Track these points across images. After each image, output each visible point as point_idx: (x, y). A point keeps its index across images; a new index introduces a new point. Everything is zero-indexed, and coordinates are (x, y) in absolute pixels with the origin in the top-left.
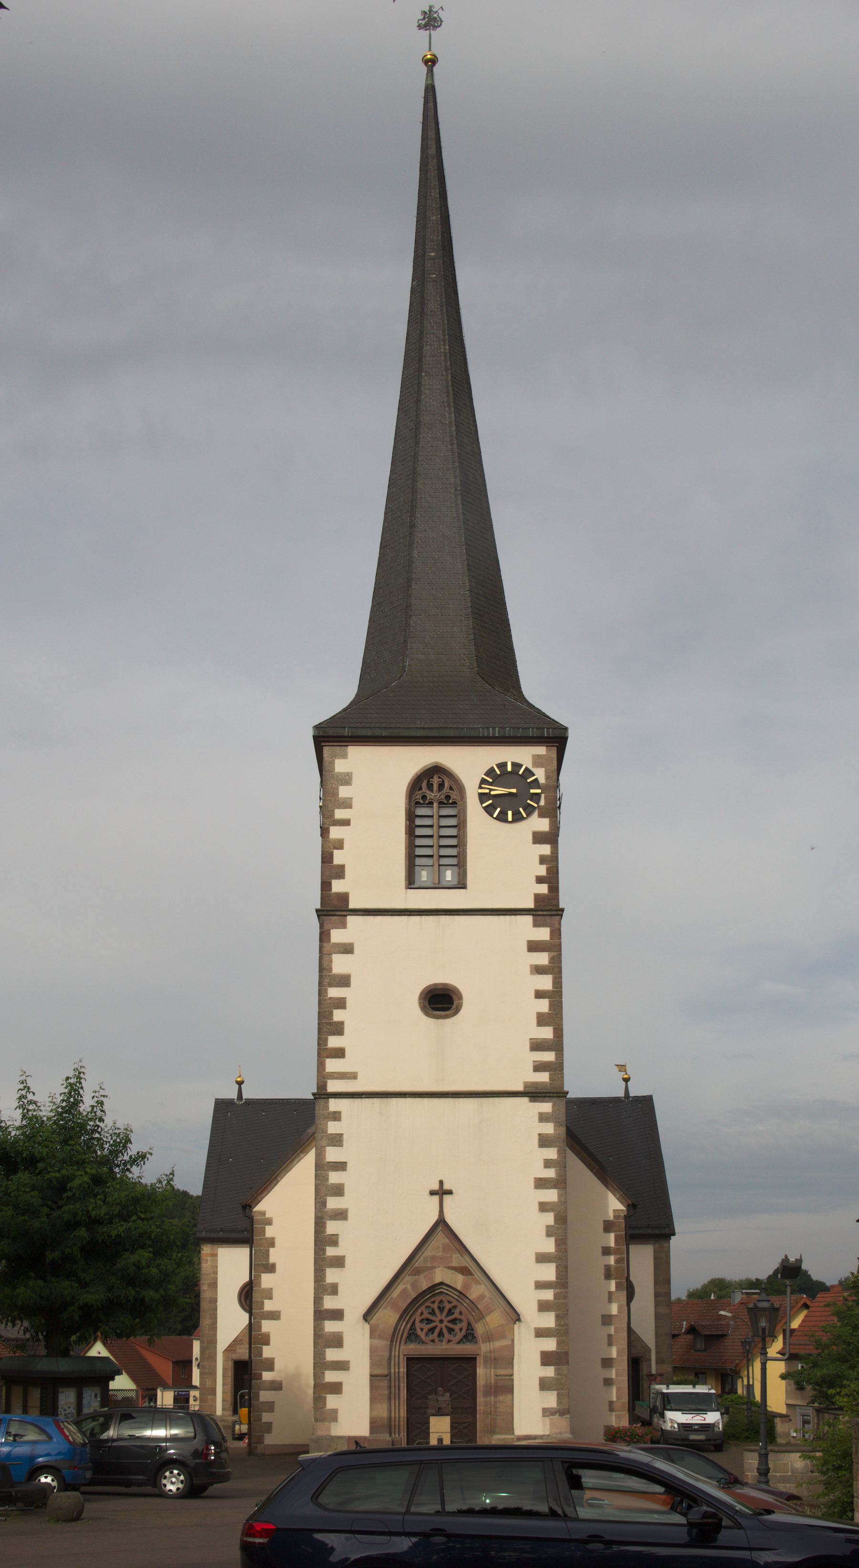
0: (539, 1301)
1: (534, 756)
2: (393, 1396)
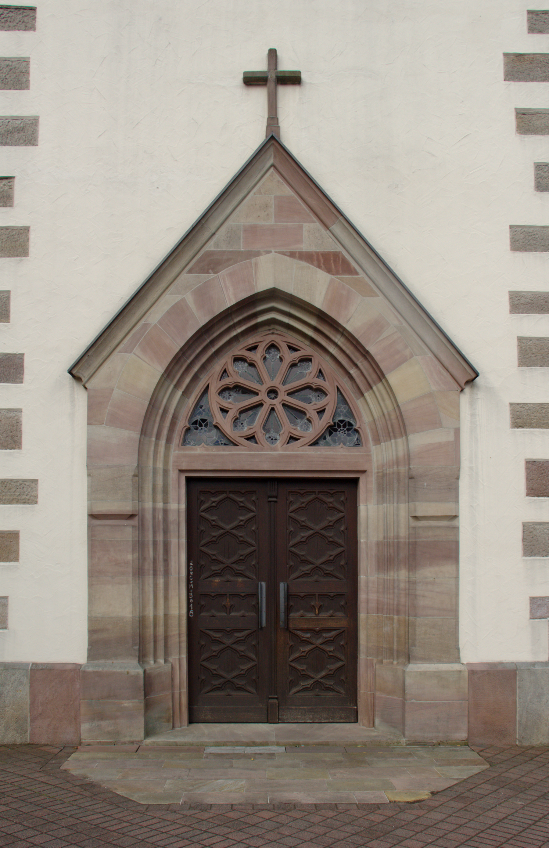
0: (520, 340)
1: (186, 477)
2: (148, 566)
